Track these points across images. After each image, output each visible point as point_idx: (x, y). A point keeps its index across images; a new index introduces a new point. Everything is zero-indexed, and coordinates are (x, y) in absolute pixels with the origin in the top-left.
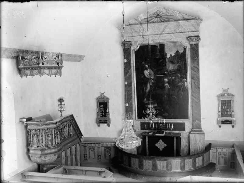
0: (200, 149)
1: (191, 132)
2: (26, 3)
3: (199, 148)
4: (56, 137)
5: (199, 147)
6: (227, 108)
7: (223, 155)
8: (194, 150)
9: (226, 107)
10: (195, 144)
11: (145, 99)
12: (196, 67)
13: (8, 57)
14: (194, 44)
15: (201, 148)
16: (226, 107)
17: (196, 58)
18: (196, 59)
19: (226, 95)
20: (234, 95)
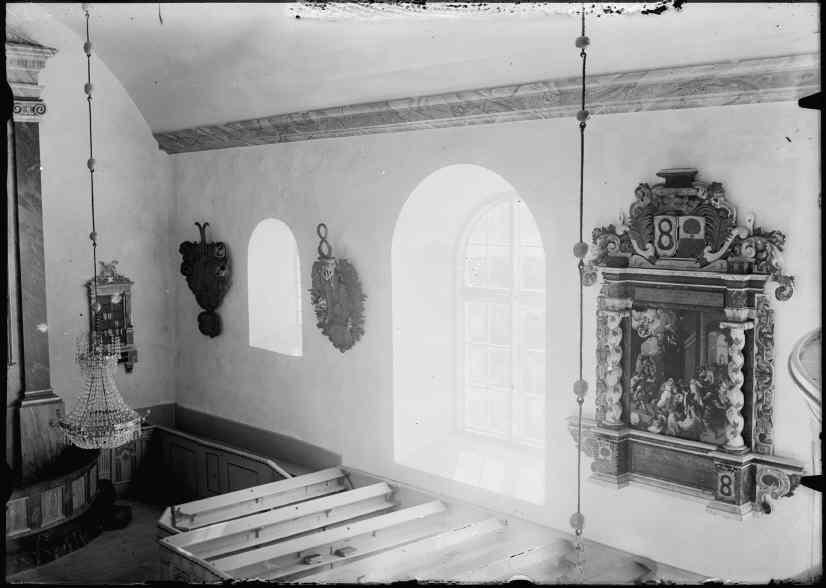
0: (51, 451)
1: (24, 403)
2: (727, 581)
3: (48, 448)
4: (614, 107)
5: (50, 442)
6: (114, 319)
7: (128, 453)
8: (35, 459)
9: (110, 316)
10: (38, 436)
11: (40, 331)
12: (33, 196)
13: (734, 363)
14: (27, 123)
15: (54, 446)
16: (110, 316)
17: (33, 168)
18: (31, 171)
19: (110, 280)
20: (132, 280)
